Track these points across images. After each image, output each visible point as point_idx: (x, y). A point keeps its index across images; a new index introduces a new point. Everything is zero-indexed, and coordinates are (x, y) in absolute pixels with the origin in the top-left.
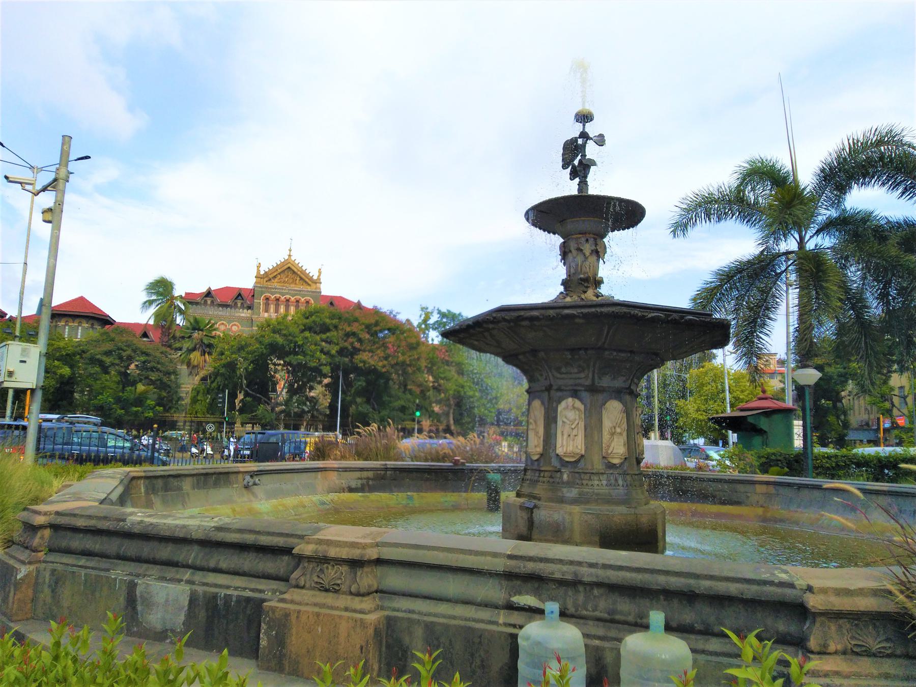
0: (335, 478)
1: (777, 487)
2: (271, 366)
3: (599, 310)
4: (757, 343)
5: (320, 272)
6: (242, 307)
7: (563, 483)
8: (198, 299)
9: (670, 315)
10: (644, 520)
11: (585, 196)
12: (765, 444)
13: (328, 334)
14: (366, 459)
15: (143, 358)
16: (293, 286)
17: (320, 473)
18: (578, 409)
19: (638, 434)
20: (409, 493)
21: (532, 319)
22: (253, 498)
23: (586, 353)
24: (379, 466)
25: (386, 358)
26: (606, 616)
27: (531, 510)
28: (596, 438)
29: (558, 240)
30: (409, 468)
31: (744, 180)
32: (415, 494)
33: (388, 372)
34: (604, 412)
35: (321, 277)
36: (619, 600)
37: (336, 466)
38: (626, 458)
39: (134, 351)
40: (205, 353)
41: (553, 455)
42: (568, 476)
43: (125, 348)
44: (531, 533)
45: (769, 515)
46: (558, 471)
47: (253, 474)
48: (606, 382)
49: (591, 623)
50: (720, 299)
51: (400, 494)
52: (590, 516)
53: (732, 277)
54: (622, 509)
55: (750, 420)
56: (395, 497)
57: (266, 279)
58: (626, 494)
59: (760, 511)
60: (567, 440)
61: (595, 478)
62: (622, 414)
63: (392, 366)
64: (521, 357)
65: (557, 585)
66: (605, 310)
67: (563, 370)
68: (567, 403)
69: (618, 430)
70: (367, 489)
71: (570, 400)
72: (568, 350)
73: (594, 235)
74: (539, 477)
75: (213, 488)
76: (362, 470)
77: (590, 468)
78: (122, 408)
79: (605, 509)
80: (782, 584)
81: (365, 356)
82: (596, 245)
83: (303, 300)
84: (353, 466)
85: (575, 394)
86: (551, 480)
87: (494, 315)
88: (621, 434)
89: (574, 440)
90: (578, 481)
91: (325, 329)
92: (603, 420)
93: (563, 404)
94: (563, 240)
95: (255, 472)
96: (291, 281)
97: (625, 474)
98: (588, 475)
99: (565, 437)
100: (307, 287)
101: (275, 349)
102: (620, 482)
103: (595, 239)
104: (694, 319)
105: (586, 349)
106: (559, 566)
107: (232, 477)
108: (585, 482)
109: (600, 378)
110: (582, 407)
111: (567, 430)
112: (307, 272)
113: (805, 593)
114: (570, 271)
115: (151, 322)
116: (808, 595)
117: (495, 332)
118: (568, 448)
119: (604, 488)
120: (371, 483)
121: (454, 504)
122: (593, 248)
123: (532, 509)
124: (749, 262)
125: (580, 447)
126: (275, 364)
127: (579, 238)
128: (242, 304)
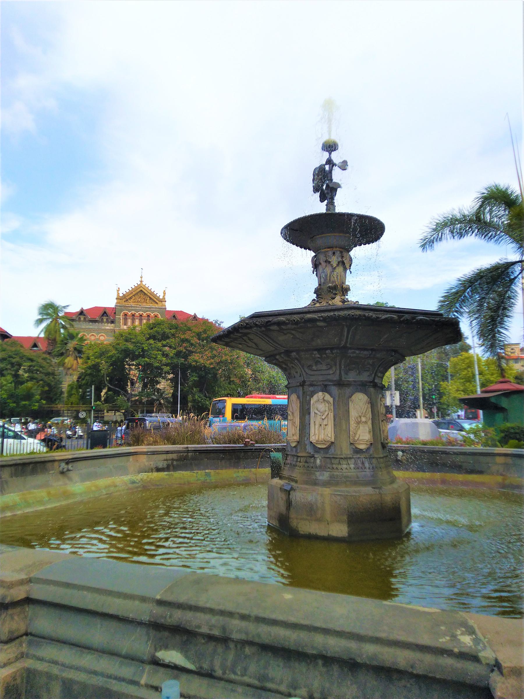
0: (145, 460)
1: (514, 459)
2: (127, 366)
3: (336, 313)
4: (499, 337)
5: (164, 293)
6: (107, 322)
7: (316, 467)
8: (74, 317)
9: (403, 316)
10: (388, 499)
11: (332, 214)
12: (506, 419)
13: (167, 341)
14: (174, 443)
15: (29, 364)
16: (145, 305)
17: (131, 457)
18: (328, 402)
19: (382, 421)
20: (207, 471)
21: (279, 324)
22: (67, 482)
23: (331, 352)
24: (181, 449)
25: (213, 357)
26: (256, 682)
27: (288, 492)
28: (344, 427)
29: (311, 254)
30: (207, 450)
31: (483, 202)
32: (212, 471)
33: (214, 368)
34: (350, 403)
35: (166, 297)
36: (271, 662)
37: (145, 450)
38: (371, 444)
39: (21, 358)
40: (77, 357)
41: (307, 442)
42: (321, 461)
43: (14, 356)
44: (288, 512)
45: (507, 482)
46: (312, 457)
47: (68, 462)
48: (352, 377)
49: (240, 689)
50: (463, 300)
51: (199, 472)
52: (339, 497)
53: (474, 283)
54: (369, 490)
55: (493, 400)
56: (195, 474)
57: (125, 300)
58: (372, 476)
59: (499, 479)
60: (319, 429)
61: (344, 463)
62: (367, 404)
63: (218, 364)
64: (277, 357)
65: (206, 640)
66: (342, 313)
67: (314, 368)
68: (318, 396)
69: (363, 419)
70: (171, 468)
71: (320, 394)
72: (316, 350)
73: (341, 248)
74: (297, 461)
75: (31, 475)
76: (167, 452)
77: (339, 453)
78: (14, 402)
79: (353, 490)
80: (463, 656)
81: (195, 357)
82: (342, 257)
83: (130, 313)
84: (160, 450)
85: (325, 389)
86: (306, 465)
87: (247, 321)
88: (366, 422)
89: (324, 429)
90: (329, 466)
91: (165, 337)
92: (350, 410)
93: (315, 398)
94: (315, 254)
95: (70, 459)
96: (143, 301)
97: (371, 458)
98: (338, 460)
99: (317, 426)
100: (156, 305)
101: (127, 353)
102: (367, 465)
103: (341, 252)
104: (425, 319)
105: (332, 349)
106: (208, 617)
107: (49, 465)
108: (334, 466)
109: (347, 374)
110: (331, 400)
111: (318, 420)
112: (155, 293)
113: (492, 671)
114: (321, 282)
115: (42, 335)
116: (495, 677)
117: (251, 336)
118: (320, 436)
119: (353, 471)
120: (175, 463)
121: (244, 478)
122: (340, 259)
123: (289, 492)
124: (488, 269)
125: (330, 435)
126: (129, 365)
127: (327, 251)
128: (107, 319)
